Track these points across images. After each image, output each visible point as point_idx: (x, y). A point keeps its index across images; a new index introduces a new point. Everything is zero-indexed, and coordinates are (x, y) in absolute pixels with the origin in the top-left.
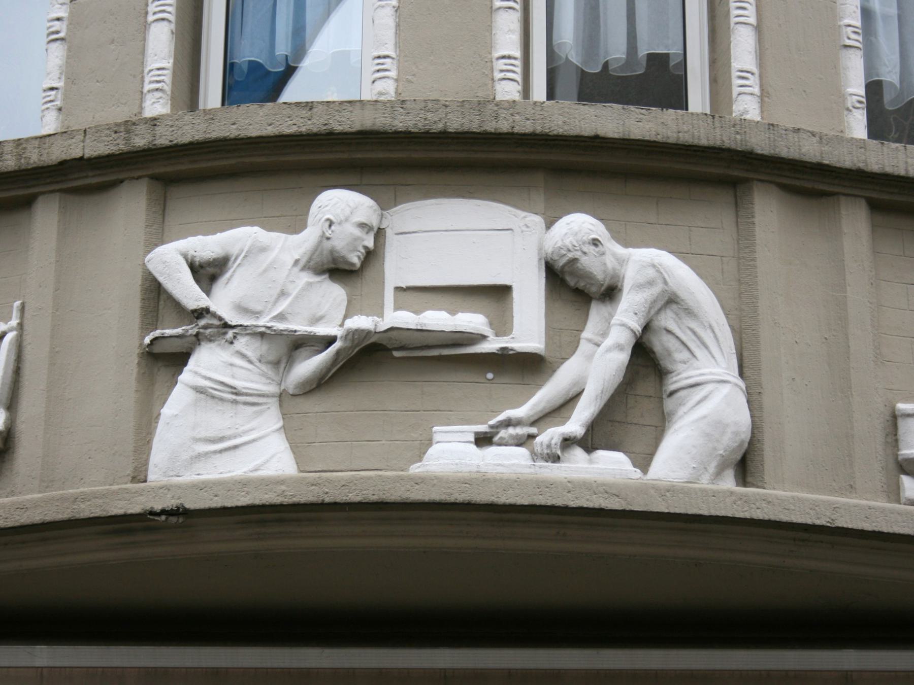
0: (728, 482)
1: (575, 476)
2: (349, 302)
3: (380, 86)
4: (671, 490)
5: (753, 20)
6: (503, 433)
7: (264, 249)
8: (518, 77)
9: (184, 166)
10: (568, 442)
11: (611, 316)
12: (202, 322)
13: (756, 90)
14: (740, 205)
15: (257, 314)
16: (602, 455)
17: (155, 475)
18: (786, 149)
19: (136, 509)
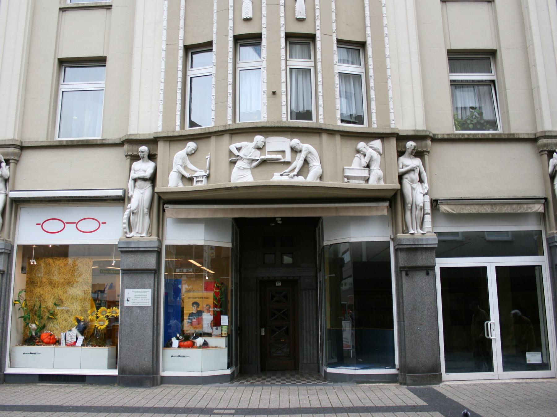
0: (318, 181)
1: (295, 181)
2: (261, 153)
3: (264, 119)
4: (310, 182)
5: (322, 106)
6: (284, 174)
7: (247, 146)
8: (286, 117)
9: (234, 132)
10: (294, 175)
11: (301, 155)
12: (239, 157)
13: (323, 118)
14: (320, 136)
15: (247, 156)
16: (299, 177)
17: (232, 181)
18: (327, 128)
19: (229, 186)
